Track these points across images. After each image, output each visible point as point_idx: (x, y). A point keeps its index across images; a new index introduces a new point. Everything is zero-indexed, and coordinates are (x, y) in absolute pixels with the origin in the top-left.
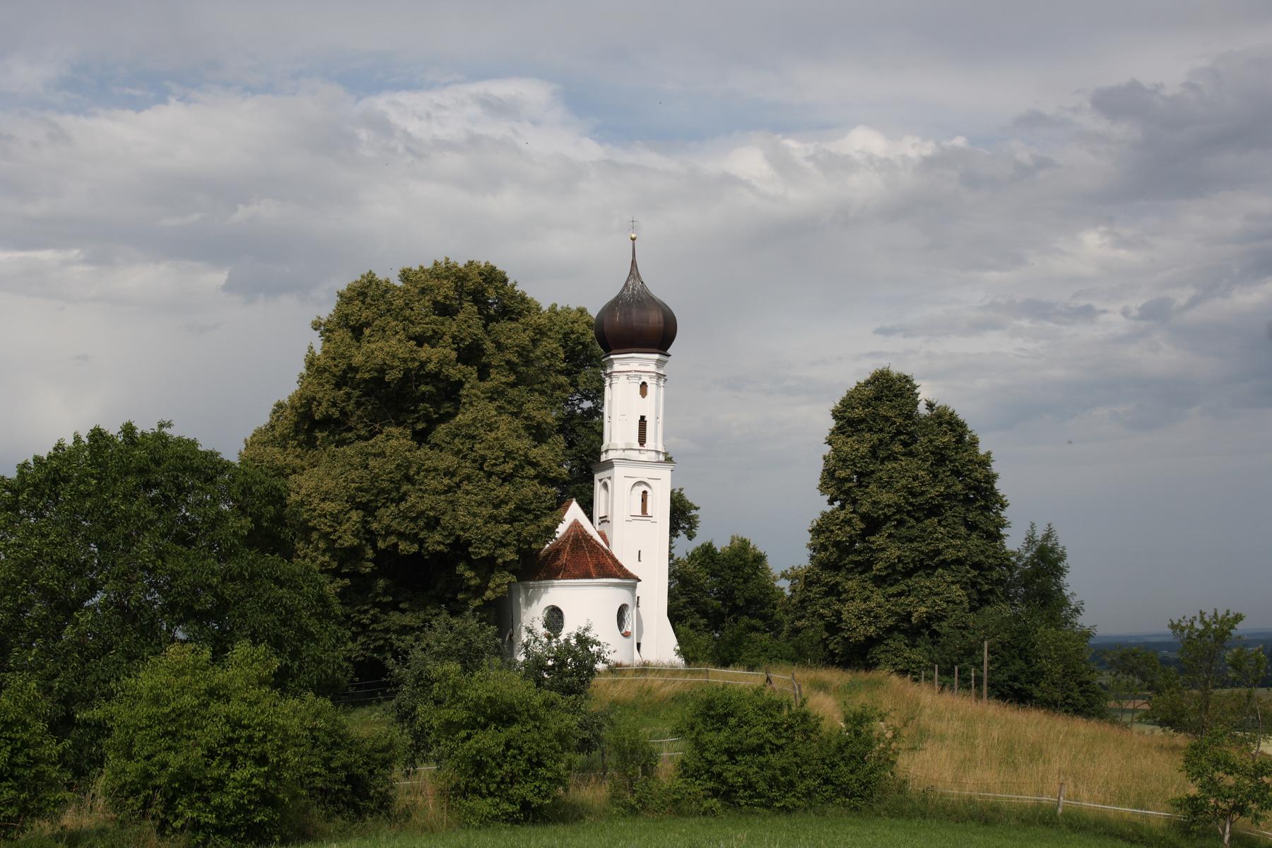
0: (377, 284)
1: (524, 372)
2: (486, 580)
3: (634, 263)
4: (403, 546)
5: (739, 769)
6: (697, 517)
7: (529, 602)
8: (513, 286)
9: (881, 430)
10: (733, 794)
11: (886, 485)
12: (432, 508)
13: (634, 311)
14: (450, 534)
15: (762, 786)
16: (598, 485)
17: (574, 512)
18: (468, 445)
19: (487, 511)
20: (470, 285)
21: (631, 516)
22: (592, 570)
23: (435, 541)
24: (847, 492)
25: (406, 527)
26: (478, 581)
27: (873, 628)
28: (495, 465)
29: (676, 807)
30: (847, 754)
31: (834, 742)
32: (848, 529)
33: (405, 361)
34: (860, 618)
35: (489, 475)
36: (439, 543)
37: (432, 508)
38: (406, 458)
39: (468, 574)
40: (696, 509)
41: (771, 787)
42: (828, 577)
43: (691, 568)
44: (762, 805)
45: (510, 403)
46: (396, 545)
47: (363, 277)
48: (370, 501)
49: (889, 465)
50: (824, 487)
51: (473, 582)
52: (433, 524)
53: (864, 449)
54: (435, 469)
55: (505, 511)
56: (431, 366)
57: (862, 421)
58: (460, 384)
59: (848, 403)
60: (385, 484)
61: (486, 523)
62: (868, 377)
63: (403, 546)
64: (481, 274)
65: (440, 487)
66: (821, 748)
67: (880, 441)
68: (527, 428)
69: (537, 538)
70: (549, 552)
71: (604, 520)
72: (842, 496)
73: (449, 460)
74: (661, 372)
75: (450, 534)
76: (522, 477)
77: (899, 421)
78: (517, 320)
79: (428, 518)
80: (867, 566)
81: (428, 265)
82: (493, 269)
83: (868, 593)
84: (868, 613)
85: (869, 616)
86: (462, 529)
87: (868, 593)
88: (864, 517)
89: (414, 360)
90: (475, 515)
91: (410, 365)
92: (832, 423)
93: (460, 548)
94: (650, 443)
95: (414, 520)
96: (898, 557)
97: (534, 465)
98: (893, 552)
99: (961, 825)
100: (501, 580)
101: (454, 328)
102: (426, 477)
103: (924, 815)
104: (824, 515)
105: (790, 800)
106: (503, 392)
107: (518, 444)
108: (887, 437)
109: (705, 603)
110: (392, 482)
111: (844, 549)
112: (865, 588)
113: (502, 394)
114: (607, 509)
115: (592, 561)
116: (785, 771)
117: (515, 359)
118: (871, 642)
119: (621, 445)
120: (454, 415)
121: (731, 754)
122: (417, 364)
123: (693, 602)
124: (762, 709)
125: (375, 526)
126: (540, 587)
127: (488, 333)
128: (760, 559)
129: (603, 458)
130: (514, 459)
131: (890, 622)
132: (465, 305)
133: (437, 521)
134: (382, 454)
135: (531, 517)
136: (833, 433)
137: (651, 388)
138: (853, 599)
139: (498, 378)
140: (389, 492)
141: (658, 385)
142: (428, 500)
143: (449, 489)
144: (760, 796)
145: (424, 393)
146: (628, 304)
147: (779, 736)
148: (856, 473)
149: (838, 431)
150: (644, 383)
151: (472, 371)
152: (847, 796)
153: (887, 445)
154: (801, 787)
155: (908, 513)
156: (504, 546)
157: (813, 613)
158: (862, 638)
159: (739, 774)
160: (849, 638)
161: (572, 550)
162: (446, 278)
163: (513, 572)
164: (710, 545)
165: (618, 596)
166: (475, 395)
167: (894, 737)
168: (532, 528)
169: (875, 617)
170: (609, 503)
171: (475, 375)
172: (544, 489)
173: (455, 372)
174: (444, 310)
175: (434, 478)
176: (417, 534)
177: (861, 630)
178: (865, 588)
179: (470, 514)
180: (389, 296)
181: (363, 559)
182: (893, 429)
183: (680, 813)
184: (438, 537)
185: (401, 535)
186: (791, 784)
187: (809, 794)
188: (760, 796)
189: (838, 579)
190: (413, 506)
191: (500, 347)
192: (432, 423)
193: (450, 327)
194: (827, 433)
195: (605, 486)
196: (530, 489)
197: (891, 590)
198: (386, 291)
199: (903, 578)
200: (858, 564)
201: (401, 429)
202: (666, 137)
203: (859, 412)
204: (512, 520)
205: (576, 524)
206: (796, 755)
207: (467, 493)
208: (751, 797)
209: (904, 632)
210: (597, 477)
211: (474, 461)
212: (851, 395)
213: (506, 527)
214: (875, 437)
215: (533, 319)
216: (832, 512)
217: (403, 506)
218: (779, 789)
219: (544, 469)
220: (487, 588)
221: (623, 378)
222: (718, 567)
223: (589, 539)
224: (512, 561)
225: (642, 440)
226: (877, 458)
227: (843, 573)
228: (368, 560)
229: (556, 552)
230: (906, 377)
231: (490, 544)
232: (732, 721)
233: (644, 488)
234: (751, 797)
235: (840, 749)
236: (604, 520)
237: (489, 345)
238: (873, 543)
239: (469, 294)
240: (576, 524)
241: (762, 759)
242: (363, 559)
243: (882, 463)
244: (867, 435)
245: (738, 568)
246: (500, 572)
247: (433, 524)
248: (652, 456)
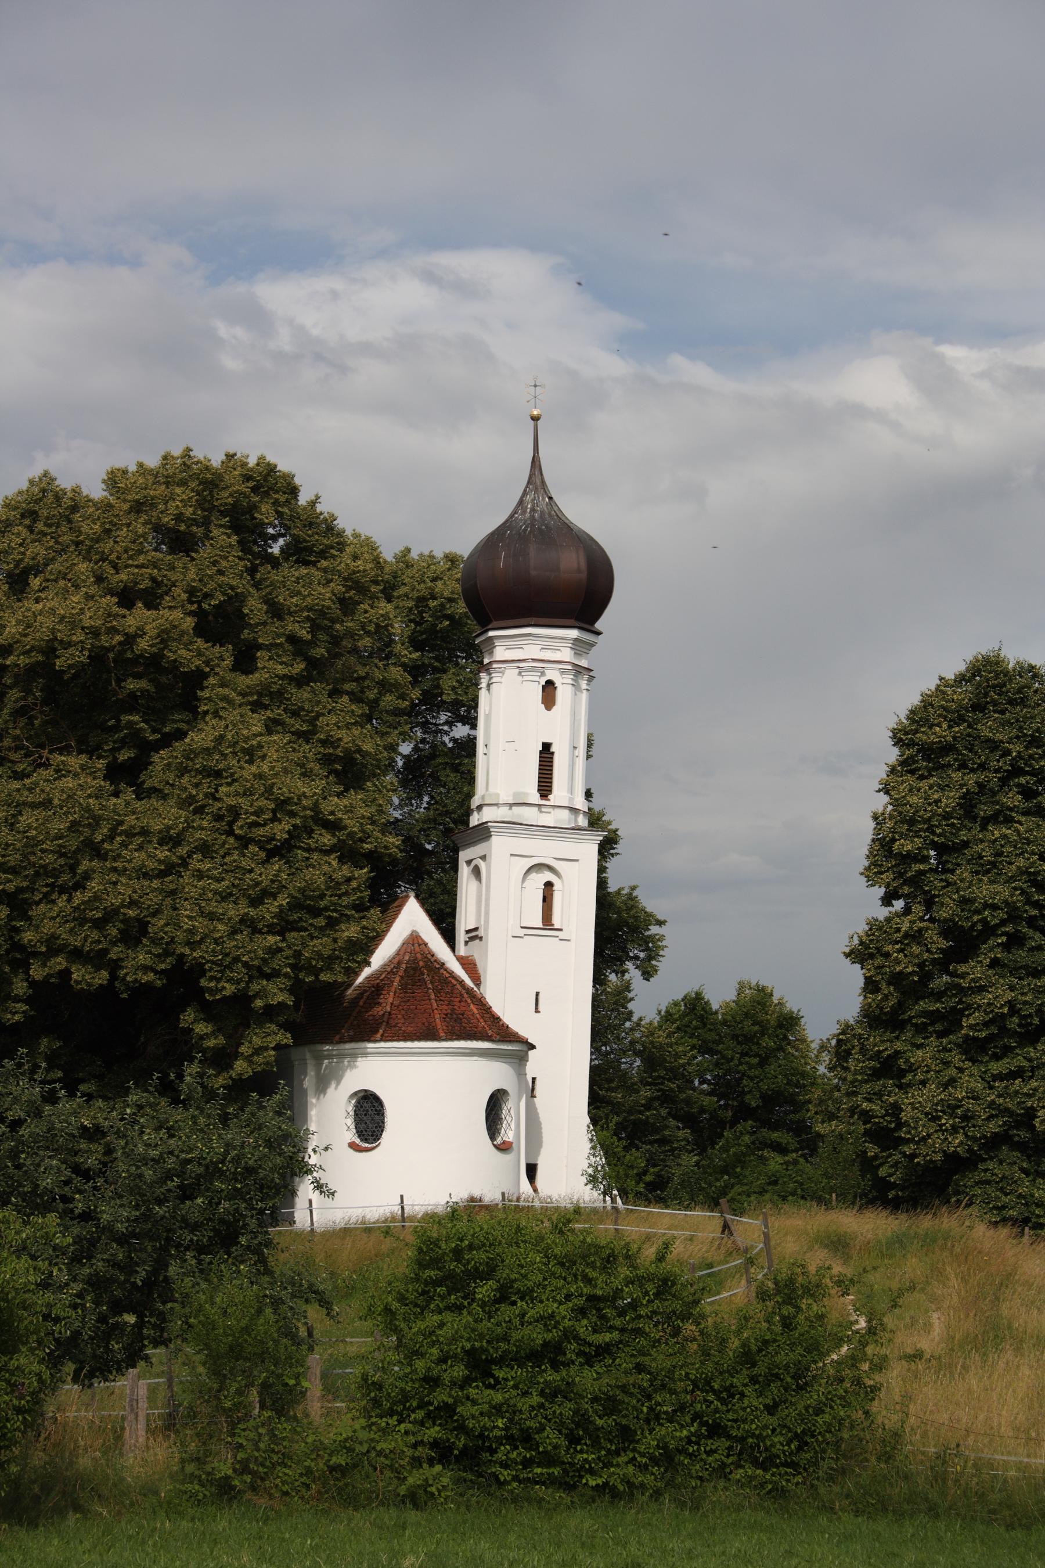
0: (58, 498)
1: (324, 656)
2: (235, 1040)
3: (536, 463)
4: (79, 974)
5: (498, 1397)
6: (662, 938)
7: (322, 1086)
8: (313, 503)
9: (983, 767)
10: (485, 1456)
11: (988, 869)
12: (133, 903)
13: (533, 550)
14: (167, 953)
15: (551, 1438)
16: (464, 872)
17: (412, 919)
18: (206, 788)
19: (235, 911)
20: (225, 497)
21: (523, 933)
22: (439, 1024)
23: (139, 965)
24: (916, 881)
25: (86, 938)
26: (221, 1040)
27: (960, 1137)
28: (256, 824)
29: (341, 1482)
30: (761, 1369)
31: (735, 1343)
32: (916, 949)
33: (95, 633)
34: (935, 1119)
35: (244, 842)
36: (146, 969)
37: (133, 903)
38: (88, 810)
39: (202, 1028)
40: (660, 923)
41: (574, 1440)
42: (881, 1043)
43: (661, 1038)
44: (550, 1482)
45: (295, 714)
46: (66, 974)
47: (31, 482)
48: (20, 890)
49: (996, 832)
50: (873, 873)
51: (211, 1043)
52: (134, 933)
53: (950, 800)
54: (144, 832)
55: (270, 910)
56: (143, 644)
57: (947, 748)
58: (197, 678)
59: (920, 717)
60: (50, 858)
61: (234, 932)
62: (962, 667)
63: (79, 974)
64: (247, 478)
65: (151, 864)
66: (706, 1353)
67: (981, 785)
68: (326, 760)
69: (330, 961)
70: (362, 989)
71: (474, 936)
72: (906, 890)
73: (167, 815)
74: (584, 663)
75: (167, 953)
76: (309, 850)
77: (1016, 748)
78: (314, 564)
79: (126, 920)
80: (951, 1020)
81: (153, 462)
82: (271, 469)
83: (953, 1072)
84: (951, 1109)
85: (953, 1115)
86: (189, 944)
87: (953, 1072)
88: (948, 930)
89: (114, 630)
90: (212, 917)
91: (105, 641)
92: (893, 754)
93: (184, 981)
94: (560, 793)
95: (99, 924)
96: (1011, 1004)
97: (333, 826)
98: (1000, 994)
99: (1019, 1534)
100: (264, 1040)
101: (192, 575)
102: (124, 845)
103: (933, 1511)
104: (874, 925)
105: (622, 1469)
106: (280, 693)
107: (300, 786)
108: (994, 778)
109: (688, 1102)
110: (62, 855)
111: (910, 988)
112: (947, 1064)
113: (278, 696)
114: (478, 919)
115: (444, 1008)
116: (610, 1405)
117: (304, 634)
118: (957, 1164)
119: (506, 797)
120: (181, 735)
121: (481, 1366)
122: (119, 638)
123: (666, 1098)
124: (566, 1262)
125: (28, 936)
126: (341, 1056)
127: (257, 585)
128: (790, 1022)
129: (474, 820)
130: (292, 814)
131: (994, 1127)
132: (215, 532)
133: (143, 926)
134: (47, 804)
135: (321, 922)
136: (893, 770)
137: (564, 692)
138: (924, 1083)
139: (270, 668)
140: (55, 873)
141: (576, 686)
142: (127, 888)
143: (168, 870)
144: (549, 1459)
145: (132, 695)
146: (522, 538)
147: (602, 1324)
148: (935, 845)
149: (905, 767)
150: (550, 684)
151: (224, 655)
152: (756, 1464)
153: (994, 794)
154: (649, 1442)
155: (1031, 922)
156: (268, 977)
157: (852, 1111)
158: (938, 1157)
159: (497, 1410)
160: (914, 1156)
161: (404, 987)
162: (183, 483)
163: (286, 1026)
164: (699, 996)
165: (495, 1074)
166: (225, 699)
167: (871, 1331)
168: (322, 944)
169: (965, 1118)
170: (483, 904)
171: (228, 662)
172: (346, 871)
173: (188, 654)
174: (181, 542)
175: (140, 848)
176: (105, 952)
177: (937, 1141)
178: (947, 1064)
179: (204, 916)
180: (77, 517)
181: (8, 997)
182: (1005, 764)
183: (352, 1501)
184: (143, 958)
185: (76, 955)
186: (626, 1436)
187: (666, 1458)
188: (549, 1459)
189: (898, 1046)
190: (96, 898)
191: (276, 611)
192: (146, 749)
193: (186, 572)
194: (882, 772)
195: (477, 872)
196: (321, 870)
197: (996, 1067)
198: (74, 508)
199: (1021, 1045)
200: (934, 1016)
201: (83, 758)
202: (733, 346)
203: (941, 733)
204: (283, 926)
205: (415, 941)
206: (640, 1368)
207: (200, 875)
208: (527, 1463)
209: (1021, 1146)
210: (464, 856)
211: (218, 818)
212: (927, 702)
213: (272, 939)
214: (971, 780)
215: (344, 562)
216: (888, 920)
217: (78, 897)
218: (596, 1444)
219: (351, 835)
220: (236, 1055)
221: (511, 672)
222: (712, 1036)
223: (435, 967)
224: (281, 1005)
225: (545, 787)
226: (974, 819)
227: (908, 1034)
228: (17, 999)
229: (376, 987)
230: (1032, 668)
231: (239, 972)
232: (485, 1290)
233: (548, 876)
234: (527, 1463)
235: (747, 1357)
236: (474, 936)
237: (254, 607)
238: (963, 976)
239: (223, 514)
240: (415, 941)
241: (551, 1376)
242: (8, 997)
243: (984, 828)
244: (956, 776)
245: (749, 1039)
246: (261, 1025)
247: (134, 933)
248: (563, 818)
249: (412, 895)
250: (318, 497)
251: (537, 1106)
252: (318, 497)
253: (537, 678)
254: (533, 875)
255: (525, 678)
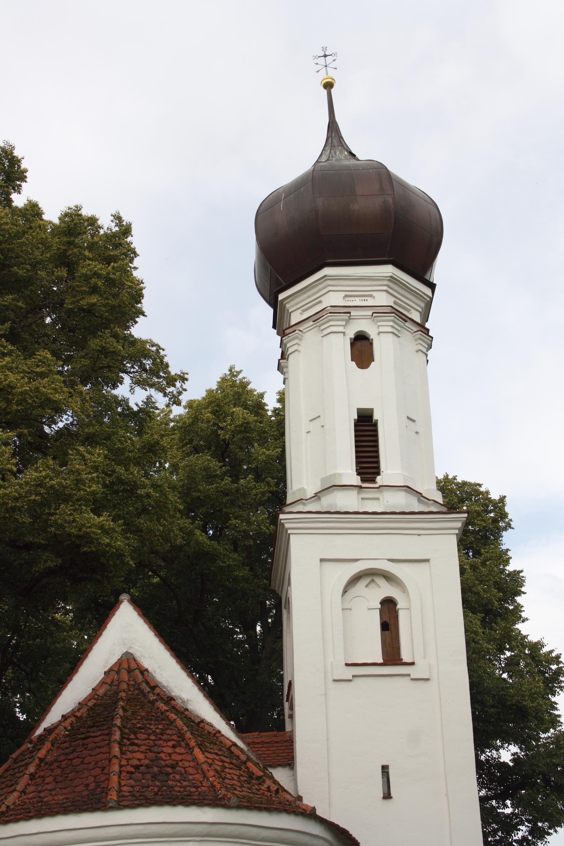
3: (333, 127)
205: (128, 668)
233: (385, 590)
240: (128, 668)
249: (271, 770)
250: (145, 316)
251: (108, 626)
252: (145, 316)
253: (341, 329)
254: (360, 588)
255: (325, 332)
